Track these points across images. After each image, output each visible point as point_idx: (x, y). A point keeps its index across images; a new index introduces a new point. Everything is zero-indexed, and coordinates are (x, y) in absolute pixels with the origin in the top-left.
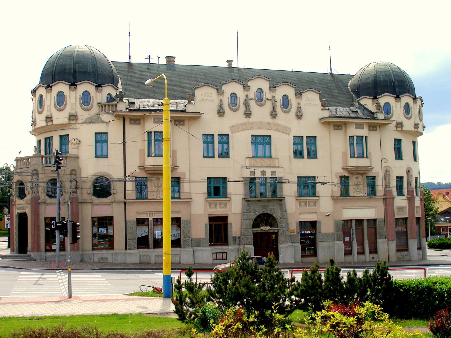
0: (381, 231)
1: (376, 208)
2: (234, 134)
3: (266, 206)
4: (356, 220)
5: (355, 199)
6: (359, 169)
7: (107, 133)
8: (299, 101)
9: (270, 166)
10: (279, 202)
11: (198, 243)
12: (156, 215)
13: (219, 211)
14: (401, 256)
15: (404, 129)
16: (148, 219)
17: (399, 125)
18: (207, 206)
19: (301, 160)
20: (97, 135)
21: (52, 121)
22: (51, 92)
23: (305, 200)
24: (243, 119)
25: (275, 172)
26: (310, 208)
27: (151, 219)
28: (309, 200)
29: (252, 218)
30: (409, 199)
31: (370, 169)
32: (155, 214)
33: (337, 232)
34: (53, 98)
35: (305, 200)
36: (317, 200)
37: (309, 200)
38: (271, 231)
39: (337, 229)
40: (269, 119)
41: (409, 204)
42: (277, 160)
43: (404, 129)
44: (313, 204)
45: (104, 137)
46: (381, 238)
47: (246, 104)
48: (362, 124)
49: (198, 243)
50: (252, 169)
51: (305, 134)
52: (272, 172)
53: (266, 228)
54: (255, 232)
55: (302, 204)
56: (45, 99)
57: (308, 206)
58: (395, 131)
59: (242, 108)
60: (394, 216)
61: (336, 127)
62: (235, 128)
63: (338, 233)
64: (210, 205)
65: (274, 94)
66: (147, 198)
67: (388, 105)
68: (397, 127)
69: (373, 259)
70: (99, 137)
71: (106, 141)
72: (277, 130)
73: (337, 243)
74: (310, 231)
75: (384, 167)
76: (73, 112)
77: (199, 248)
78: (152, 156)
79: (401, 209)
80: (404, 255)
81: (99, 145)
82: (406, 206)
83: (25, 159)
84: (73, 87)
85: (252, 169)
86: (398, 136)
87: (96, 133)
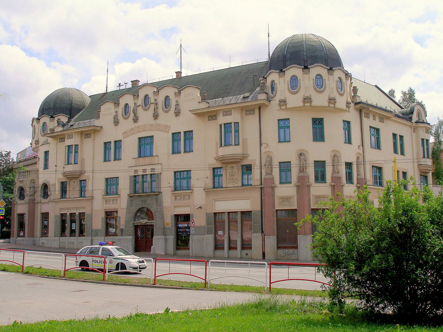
0: (255, 225)
1: (251, 199)
2: (126, 139)
3: (144, 200)
4: (241, 212)
5: (228, 190)
6: (225, 158)
7: (289, 119)
8: (177, 99)
9: (150, 163)
10: (155, 197)
11: (96, 233)
12: (71, 210)
13: (111, 207)
14: (283, 254)
15: (289, 106)
16: (75, 213)
17: (283, 102)
18: (104, 202)
19: (178, 155)
20: (280, 121)
21: (286, 105)
22: (39, 123)
23: (180, 194)
24: (133, 125)
25: (154, 169)
26: (185, 201)
27: (77, 213)
28: (185, 194)
29: (133, 212)
30: (333, 187)
31: (245, 156)
32: (71, 210)
33: (208, 225)
34: (40, 128)
35: (180, 194)
36: (190, 193)
37: (185, 194)
38: (149, 224)
39: (208, 223)
40: (152, 121)
41: (297, 192)
42: (156, 158)
43: (289, 106)
44: (188, 197)
45: (287, 123)
46: (255, 233)
47: (135, 112)
48: (89, 132)
49: (96, 233)
50: (136, 168)
51: (182, 130)
52: (151, 169)
53: (144, 221)
54: (136, 224)
55: (179, 198)
56: (278, 84)
57: (182, 200)
58: (279, 110)
59: (132, 115)
60: (274, 207)
61: (210, 118)
62: (126, 134)
63: (208, 226)
64: (106, 201)
65: (156, 98)
66: (85, 197)
67: (295, 78)
68: (280, 106)
69: (246, 256)
70: (282, 123)
71: (289, 127)
72: (159, 130)
73: (207, 236)
74: (187, 224)
75: (264, 153)
76: (307, 95)
77: (96, 238)
78: (71, 164)
79: (287, 199)
80: (289, 253)
81: (282, 131)
82: (294, 196)
83: (23, 172)
84: (281, 74)
85: (136, 168)
86: (283, 115)
87: (279, 120)
